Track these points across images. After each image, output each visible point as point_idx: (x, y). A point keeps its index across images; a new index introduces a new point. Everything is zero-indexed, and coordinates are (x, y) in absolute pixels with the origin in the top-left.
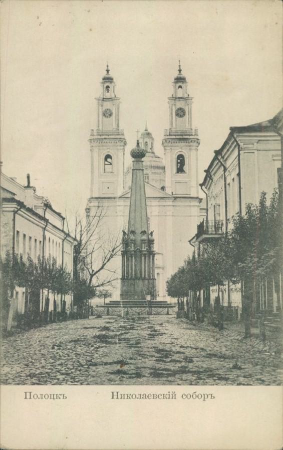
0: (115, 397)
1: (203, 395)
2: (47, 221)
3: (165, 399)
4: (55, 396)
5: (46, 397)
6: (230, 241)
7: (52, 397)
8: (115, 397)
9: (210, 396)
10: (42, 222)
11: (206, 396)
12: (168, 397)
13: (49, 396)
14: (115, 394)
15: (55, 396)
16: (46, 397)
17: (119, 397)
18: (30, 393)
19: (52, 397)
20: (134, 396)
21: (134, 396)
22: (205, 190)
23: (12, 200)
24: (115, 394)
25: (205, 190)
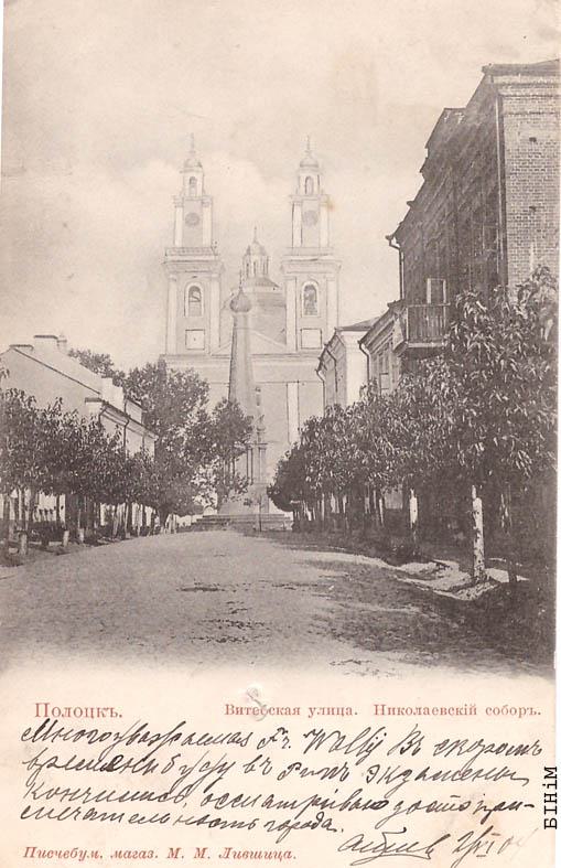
0: (380, 712)
1: (84, 711)
2: (128, 417)
3: (459, 716)
4: (95, 712)
5: (78, 713)
6: (463, 621)
7: (89, 714)
8: (380, 712)
9: (529, 712)
10: (124, 418)
11: (523, 711)
12: (463, 712)
13: (84, 711)
14: (380, 708)
15: (95, 712)
16: (78, 713)
17: (386, 711)
18: (46, 705)
19: (89, 714)
20: (409, 711)
21: (409, 711)
22: (322, 376)
23: (99, 400)
24: (380, 708)
25: (322, 376)
